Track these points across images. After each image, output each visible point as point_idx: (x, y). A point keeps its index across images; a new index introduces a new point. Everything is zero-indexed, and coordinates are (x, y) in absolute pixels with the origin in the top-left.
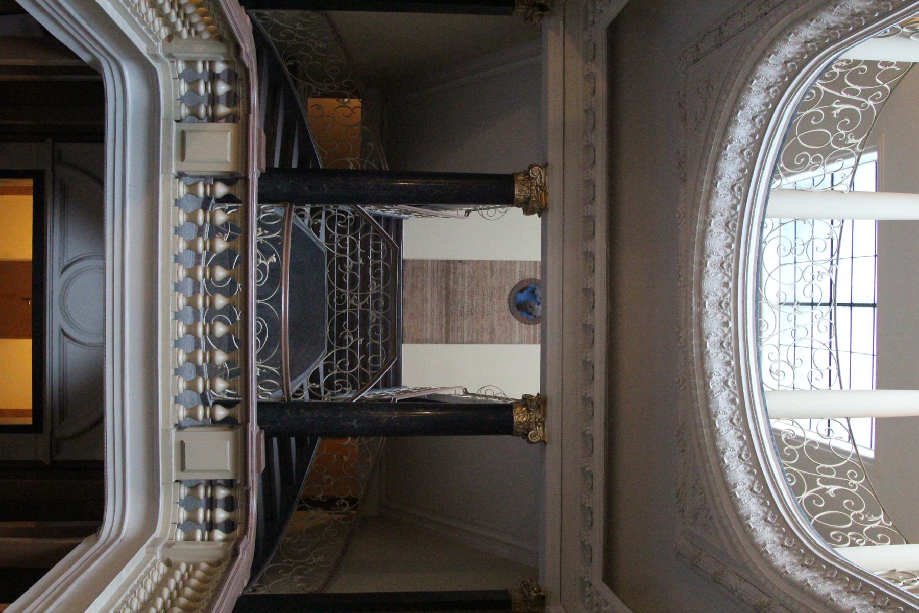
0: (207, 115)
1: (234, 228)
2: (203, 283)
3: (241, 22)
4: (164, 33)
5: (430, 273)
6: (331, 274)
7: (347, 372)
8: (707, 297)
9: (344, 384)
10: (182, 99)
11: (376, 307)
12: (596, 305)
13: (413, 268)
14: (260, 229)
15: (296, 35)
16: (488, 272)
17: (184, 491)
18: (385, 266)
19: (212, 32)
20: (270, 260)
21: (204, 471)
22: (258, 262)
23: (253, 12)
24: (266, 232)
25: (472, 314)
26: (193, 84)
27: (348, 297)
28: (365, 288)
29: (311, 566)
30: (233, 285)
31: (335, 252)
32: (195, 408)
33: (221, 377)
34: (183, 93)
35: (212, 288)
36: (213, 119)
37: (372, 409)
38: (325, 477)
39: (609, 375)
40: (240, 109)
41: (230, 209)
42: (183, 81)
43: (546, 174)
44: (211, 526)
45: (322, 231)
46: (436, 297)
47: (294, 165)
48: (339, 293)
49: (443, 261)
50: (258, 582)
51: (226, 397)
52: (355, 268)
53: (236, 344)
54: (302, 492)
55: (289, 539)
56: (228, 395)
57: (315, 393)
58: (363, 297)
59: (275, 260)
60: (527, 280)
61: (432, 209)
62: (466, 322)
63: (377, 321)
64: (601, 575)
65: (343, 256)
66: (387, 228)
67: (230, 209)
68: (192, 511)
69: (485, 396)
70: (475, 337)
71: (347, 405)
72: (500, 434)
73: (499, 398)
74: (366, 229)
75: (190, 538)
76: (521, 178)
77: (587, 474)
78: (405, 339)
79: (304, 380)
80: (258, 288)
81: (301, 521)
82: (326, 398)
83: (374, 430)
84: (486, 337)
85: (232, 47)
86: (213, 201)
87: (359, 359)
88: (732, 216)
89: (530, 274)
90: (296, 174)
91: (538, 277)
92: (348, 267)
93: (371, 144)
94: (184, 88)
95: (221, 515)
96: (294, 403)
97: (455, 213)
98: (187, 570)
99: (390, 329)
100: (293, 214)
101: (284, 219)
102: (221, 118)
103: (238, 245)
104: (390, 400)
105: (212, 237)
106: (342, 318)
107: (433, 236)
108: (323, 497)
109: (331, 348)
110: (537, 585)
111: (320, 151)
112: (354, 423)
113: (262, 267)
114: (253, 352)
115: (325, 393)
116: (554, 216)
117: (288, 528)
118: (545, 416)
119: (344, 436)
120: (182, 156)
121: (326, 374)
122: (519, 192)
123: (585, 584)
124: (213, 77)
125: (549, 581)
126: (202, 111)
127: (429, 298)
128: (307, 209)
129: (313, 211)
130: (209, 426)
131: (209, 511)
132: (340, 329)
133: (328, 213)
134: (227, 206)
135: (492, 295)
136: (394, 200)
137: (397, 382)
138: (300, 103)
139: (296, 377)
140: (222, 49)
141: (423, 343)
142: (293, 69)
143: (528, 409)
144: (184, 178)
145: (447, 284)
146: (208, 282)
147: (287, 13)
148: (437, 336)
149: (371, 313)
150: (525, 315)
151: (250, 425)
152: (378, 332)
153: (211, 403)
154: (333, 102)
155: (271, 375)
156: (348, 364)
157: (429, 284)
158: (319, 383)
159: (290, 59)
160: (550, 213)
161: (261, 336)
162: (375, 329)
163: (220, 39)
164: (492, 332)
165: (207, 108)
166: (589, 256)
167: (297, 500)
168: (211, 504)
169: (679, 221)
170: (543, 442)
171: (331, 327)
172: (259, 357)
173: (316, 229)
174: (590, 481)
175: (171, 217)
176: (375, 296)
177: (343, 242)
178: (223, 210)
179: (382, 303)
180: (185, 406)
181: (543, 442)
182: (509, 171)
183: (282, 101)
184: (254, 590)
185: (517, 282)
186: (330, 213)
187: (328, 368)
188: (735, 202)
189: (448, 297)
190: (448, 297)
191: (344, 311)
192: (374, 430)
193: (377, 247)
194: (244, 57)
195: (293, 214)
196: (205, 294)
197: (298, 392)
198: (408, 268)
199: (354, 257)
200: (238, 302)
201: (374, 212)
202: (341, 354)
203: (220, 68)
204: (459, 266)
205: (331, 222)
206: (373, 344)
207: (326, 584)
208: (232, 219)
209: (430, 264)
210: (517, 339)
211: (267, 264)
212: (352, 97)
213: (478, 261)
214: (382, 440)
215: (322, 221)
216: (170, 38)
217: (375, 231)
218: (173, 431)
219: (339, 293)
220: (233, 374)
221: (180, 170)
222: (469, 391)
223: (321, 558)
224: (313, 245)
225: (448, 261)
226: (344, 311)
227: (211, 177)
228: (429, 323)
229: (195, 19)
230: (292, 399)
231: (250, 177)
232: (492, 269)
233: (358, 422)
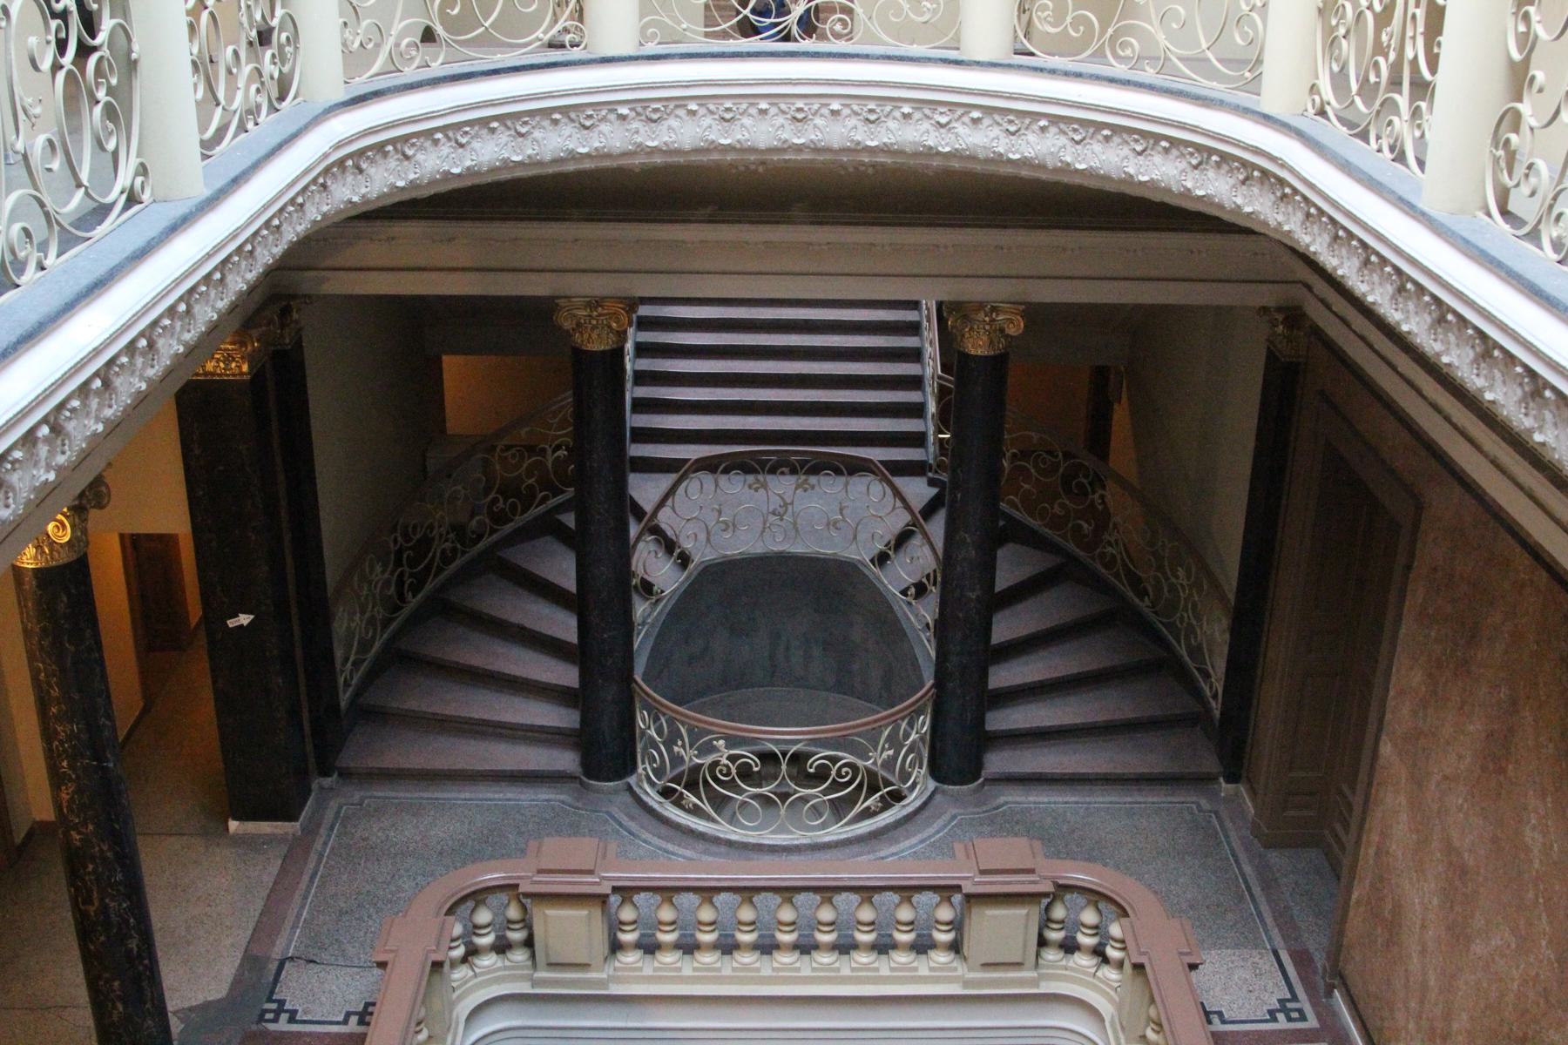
17: (1051, 955)
21: (1025, 946)
29: (1191, 595)
88: (638, 114)
118: (981, 306)
188: (612, 117)
223: (1181, 572)
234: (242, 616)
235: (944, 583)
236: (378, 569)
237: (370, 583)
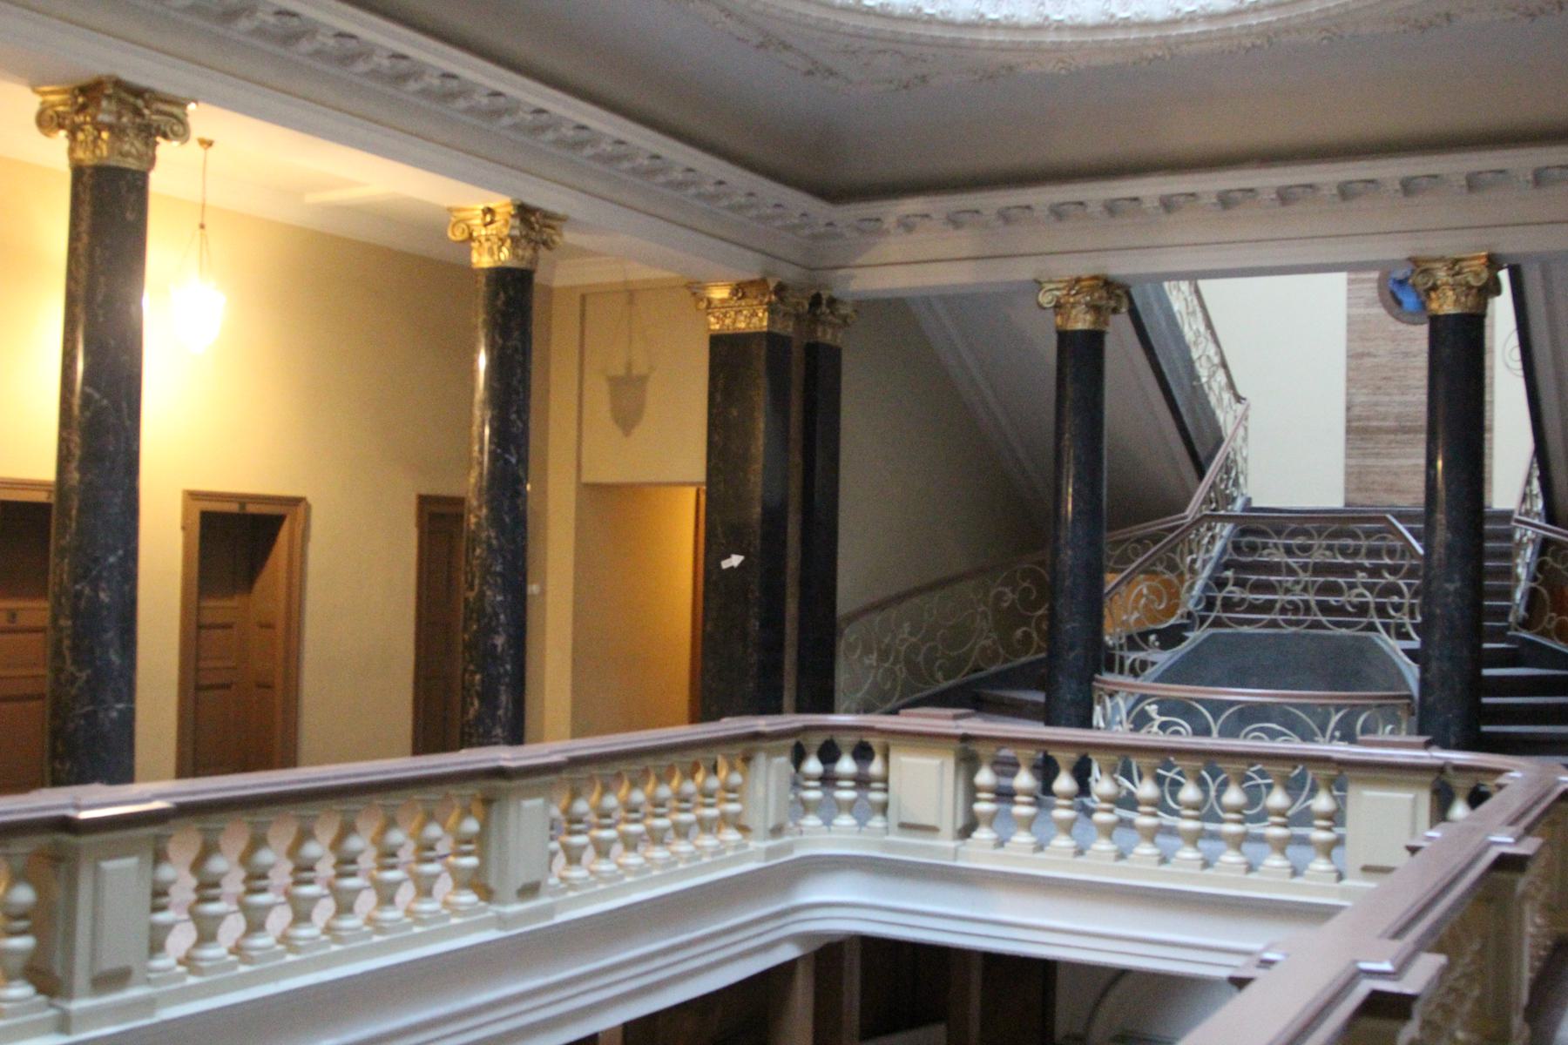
4: (731, 835)
5: (1369, 462)
8: (1178, 11)
11: (1305, 549)
12: (1431, 172)
13: (1359, 490)
16: (1368, 362)
20: (1154, 715)
28: (1273, 568)
36: (1335, 818)
43: (1050, 282)
48: (1283, 611)
49: (1347, 440)
52: (1240, 583)
58: (1291, 571)
60: (1381, 294)
63: (1330, 548)
65: (1219, 603)
80: (1196, 733)
87: (1389, 578)
91: (1375, 275)
106: (1325, 608)
118: (1441, 259)
120: (931, 830)
131: (1142, 809)
132: (1340, 610)
135: (1406, 354)
145: (1388, 431)
149: (1317, 557)
152: (1347, 547)
157: (1387, 462)
159: (932, 676)
161: (1273, 735)
163: (747, 759)
168: (1005, 795)
171: (1338, 624)
172: (1307, 736)
175: (1018, 852)
176: (1289, 551)
179: (1299, 541)
198: (1360, 498)
202: (1381, 610)
204: (1356, 411)
208: (1110, 770)
209: (1353, 462)
211: (1160, 719)
213: (1349, 380)
216: (743, 829)
218: (1346, 883)
225: (1349, 430)
226: (1313, 604)
232: (1362, 355)
233: (1450, 580)
236: (906, 626)
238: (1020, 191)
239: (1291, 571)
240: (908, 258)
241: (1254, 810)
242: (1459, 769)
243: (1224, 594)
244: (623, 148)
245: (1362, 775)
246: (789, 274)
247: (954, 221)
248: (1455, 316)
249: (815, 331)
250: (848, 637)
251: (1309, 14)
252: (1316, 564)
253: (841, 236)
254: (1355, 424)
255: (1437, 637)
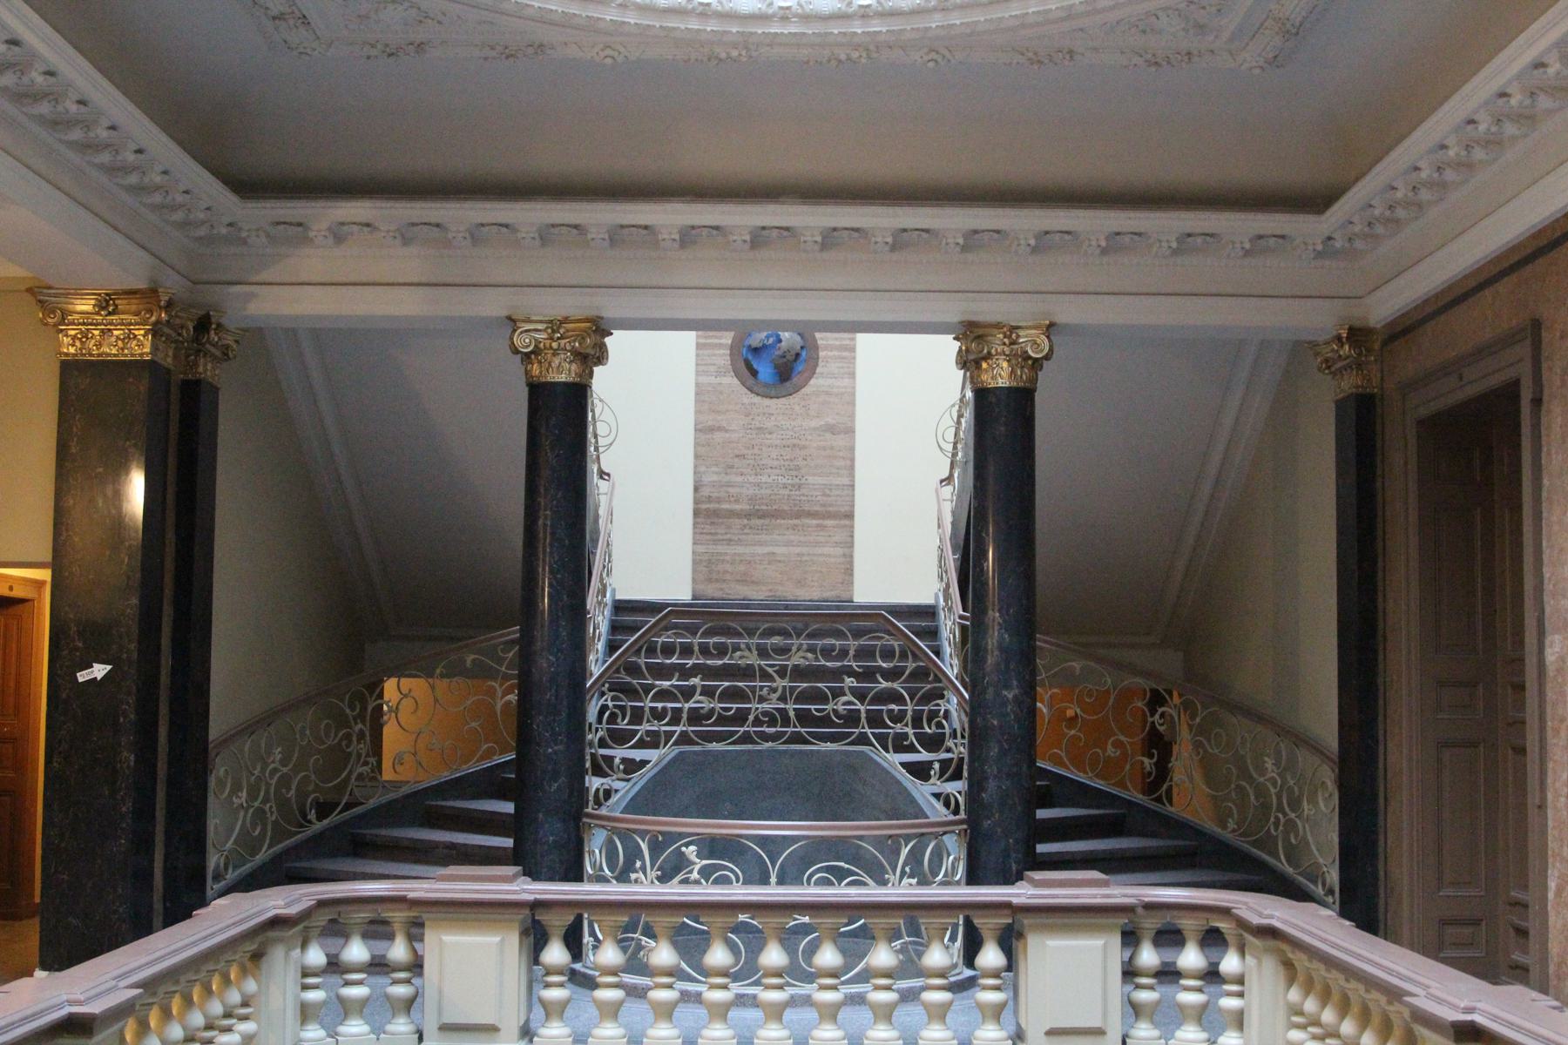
0: (408, 981)
1: (631, 927)
2: (736, 988)
3: (224, 916)
5: (720, 549)
6: (720, 737)
7: (909, 708)
9: (933, 715)
10: (378, 1030)
11: (784, 651)
12: (784, 224)
13: (710, 580)
14: (633, 876)
15: (256, 804)
16: (718, 436)
18: (707, 634)
19: (244, 972)
20: (693, 857)
22: (697, 882)
23: (212, 887)
24: (638, 864)
25: (798, 468)
26: (347, 1009)
27: (765, 706)
28: (747, 673)
29: (1284, 782)
30: (738, 929)
31: (678, 729)
32: (981, 1007)
33: (920, 955)
34: (366, 1028)
35: (747, 971)
37: (984, 660)
38: (1110, 751)
39: (916, 199)
40: (398, 916)
41: (593, 934)
42: (341, 1029)
43: (529, 321)
44: (1212, 975)
45: (638, 755)
46: (764, 537)
47: (508, 807)
48: (757, 722)
49: (695, 524)
50: (1315, 882)
51: (959, 943)
52: (708, 692)
53: (857, 925)
54: (1139, 798)
55: (1231, 825)
56: (953, 939)
57: (951, 771)
58: (765, 676)
59: (693, 848)
61: (595, 541)
62: (811, 479)
63: (811, 649)
64: (1311, 218)
65: (685, 716)
66: (633, 629)
67: (593, 934)
68: (1183, 1014)
69: (955, 444)
70: (841, 463)
71: (975, 709)
72: (1032, 413)
73: (960, 416)
74: (633, 670)
75: (1239, 1021)
76: (535, 369)
77: (1113, 244)
78: (845, 596)
79: (922, 792)
80: (748, 882)
81: (1190, 797)
82: (959, 749)
83: (1024, 658)
84: (840, 441)
85: (271, 934)
86: (578, 966)
87: (884, 684)
89: (722, 358)
90: (527, 805)
91: (727, 338)
92: (706, 704)
93: (470, 658)
94: (355, 1027)
95: (1191, 958)
96: (969, 812)
97: (603, 500)
98: (1303, 1027)
99: (828, 626)
100: (604, 811)
101: (614, 830)
102: (414, 951)
103: (662, 921)
104: (963, 628)
105: (644, 969)
106: (804, 718)
107: (646, 545)
108: (1151, 756)
109: (863, 740)
110: (1327, 343)
111: (482, 758)
112: (1010, 696)
113: (706, 873)
114: (872, 892)
115: (949, 750)
116: (609, 306)
117: (1211, 826)
118: (998, 326)
119: (1033, 711)
121: (911, 749)
122: (562, 372)
123: (1327, 250)
124: (335, 966)
125: (1320, 320)
126: (401, 991)
127: (766, 550)
128: (594, 783)
129: (598, 772)
130: (1016, 976)
131: (1183, 982)
132: (825, 721)
133: (602, 744)
134: (587, 939)
136: (578, 614)
137: (929, 612)
138: (392, 796)
139: (922, 810)
140: (277, 954)
141: (851, 563)
142: (324, 810)
143: (985, 358)
144: (533, 1025)
146: (736, 978)
147: (214, 822)
148: (839, 536)
149: (796, 660)
150: (800, 367)
151: (1015, 901)
153: (968, 973)
154: (390, 732)
155: (915, 857)
156: (893, 707)
157: (740, 549)
158: (931, 763)
159: (304, 816)
160: (605, 314)
161: (840, 875)
162: (827, 652)
163: (257, 956)
164: (831, 429)
165: (396, 982)
166: (688, 237)
167: (1153, 806)
169: (620, 59)
170: (1050, 328)
173: (632, 766)
174: (1127, 239)
176: (763, 652)
177: (658, 715)
178: (595, 947)
179: (776, 640)
180: (978, 1027)
181: (1050, 328)
182: (523, 394)
183: (384, 832)
184: (1331, 892)
185: (736, 381)
186: (601, 740)
187: (900, 745)
189: (763, 514)
190: (763, 514)
191: (792, 714)
192: (1024, 658)
193: (668, 650)
194: (293, 910)
195: (604, 811)
196: (757, 983)
197: (947, 805)
198: (711, 590)
199: (688, 693)
200: (775, 920)
201: (600, 655)
202: (875, 720)
203: (316, 956)
204: (705, 492)
205: (620, 738)
206: (857, 657)
207: (1317, 749)
209: (701, 549)
210: (846, 382)
211: (700, 863)
212: (381, 696)
213: (697, 456)
214: (1041, 641)
215: (619, 753)
217: (638, 652)
219: (757, 722)
220: (915, 931)
221: (516, 1032)
222: (946, 474)
223: (1269, 764)
224: (665, 775)
225: (696, 513)
226: (792, 714)
227: (530, 971)
228: (819, 551)
229: (216, 1008)
230: (962, 815)
231: (531, 897)
232: (712, 430)
233: (1007, 687)
234: (96, 666)
235: (972, 735)
236: (277, 753)
237: (265, 764)
238: (278, 204)
239: (765, 676)
240: (328, 280)
241: (852, 968)
242: (1151, 907)
243: (691, 704)
244: (52, 80)
245: (1060, 921)
246: (173, 284)
247: (406, 235)
248: (1009, 389)
249: (196, 364)
250: (220, 770)
251: (927, 29)
252: (796, 667)
253: (244, 242)
254: (704, 506)
255: (994, 752)
